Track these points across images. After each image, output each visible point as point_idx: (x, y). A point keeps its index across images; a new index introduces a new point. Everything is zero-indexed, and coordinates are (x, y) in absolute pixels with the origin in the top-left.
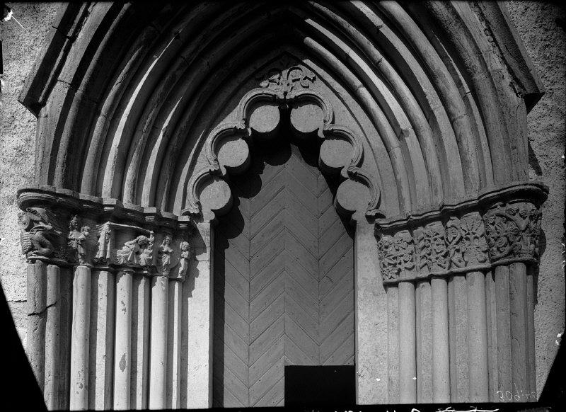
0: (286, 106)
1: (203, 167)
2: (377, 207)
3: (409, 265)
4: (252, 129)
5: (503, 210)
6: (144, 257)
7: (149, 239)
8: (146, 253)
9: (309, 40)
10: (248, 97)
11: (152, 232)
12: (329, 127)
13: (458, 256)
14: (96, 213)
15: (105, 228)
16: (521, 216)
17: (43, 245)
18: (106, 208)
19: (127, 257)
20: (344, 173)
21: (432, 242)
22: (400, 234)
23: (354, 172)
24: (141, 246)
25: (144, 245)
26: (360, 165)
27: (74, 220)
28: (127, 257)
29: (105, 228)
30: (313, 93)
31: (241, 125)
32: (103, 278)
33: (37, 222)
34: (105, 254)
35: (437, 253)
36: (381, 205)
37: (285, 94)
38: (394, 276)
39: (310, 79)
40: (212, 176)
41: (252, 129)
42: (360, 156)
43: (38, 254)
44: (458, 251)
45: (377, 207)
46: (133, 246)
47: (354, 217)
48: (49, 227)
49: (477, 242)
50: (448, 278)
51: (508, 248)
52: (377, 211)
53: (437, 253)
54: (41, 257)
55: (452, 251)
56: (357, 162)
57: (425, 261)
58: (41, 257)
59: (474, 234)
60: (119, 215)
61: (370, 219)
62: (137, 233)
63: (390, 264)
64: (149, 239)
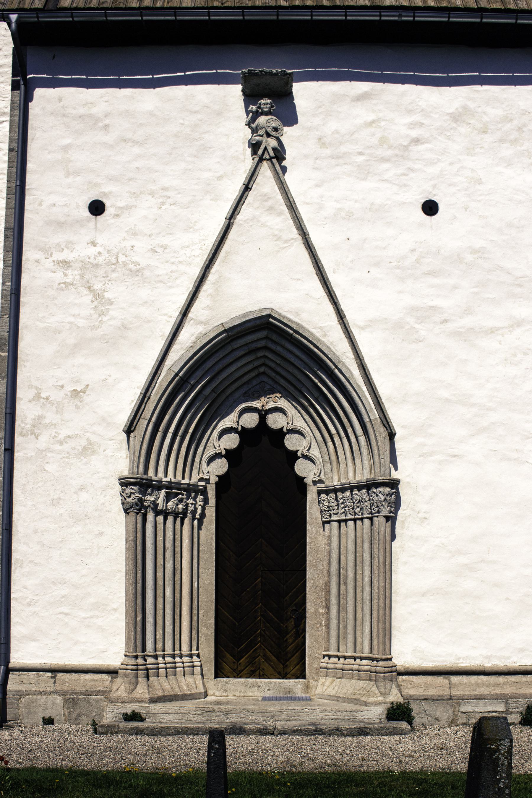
0: (263, 414)
1: (210, 452)
2: (319, 475)
3: (335, 512)
4: (241, 426)
5: (374, 490)
6: (180, 507)
7: (184, 497)
8: (183, 505)
9: (271, 320)
10: (240, 408)
11: (185, 493)
12: (290, 427)
13: (358, 510)
14: (158, 486)
15: (163, 492)
16: (382, 494)
17: (137, 505)
18: (173, 485)
19: (173, 508)
20: (299, 454)
21: (346, 500)
22: (164, 722)
23: (305, 454)
24: (179, 501)
25: (181, 501)
26: (308, 450)
27: (149, 490)
28: (173, 508)
29: (163, 492)
30: (280, 406)
31: (235, 426)
32: (160, 519)
33: (134, 493)
34: (163, 507)
35: (349, 507)
36: (322, 474)
37: (263, 406)
38: (328, 517)
39: (278, 397)
40: (217, 456)
41: (241, 426)
42: (309, 444)
43: (134, 509)
44: (358, 507)
45: (319, 475)
46: (176, 502)
47: (305, 480)
48: (140, 496)
49: (366, 504)
50: (355, 520)
51: (377, 509)
52: (319, 478)
53: (349, 507)
54: (135, 511)
55: (355, 507)
56: (307, 448)
57: (343, 510)
58: (135, 511)
59: (365, 499)
60: (169, 486)
61: (315, 483)
62: (177, 494)
63: (325, 511)
64: (184, 497)
